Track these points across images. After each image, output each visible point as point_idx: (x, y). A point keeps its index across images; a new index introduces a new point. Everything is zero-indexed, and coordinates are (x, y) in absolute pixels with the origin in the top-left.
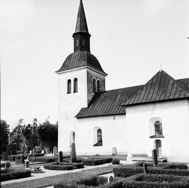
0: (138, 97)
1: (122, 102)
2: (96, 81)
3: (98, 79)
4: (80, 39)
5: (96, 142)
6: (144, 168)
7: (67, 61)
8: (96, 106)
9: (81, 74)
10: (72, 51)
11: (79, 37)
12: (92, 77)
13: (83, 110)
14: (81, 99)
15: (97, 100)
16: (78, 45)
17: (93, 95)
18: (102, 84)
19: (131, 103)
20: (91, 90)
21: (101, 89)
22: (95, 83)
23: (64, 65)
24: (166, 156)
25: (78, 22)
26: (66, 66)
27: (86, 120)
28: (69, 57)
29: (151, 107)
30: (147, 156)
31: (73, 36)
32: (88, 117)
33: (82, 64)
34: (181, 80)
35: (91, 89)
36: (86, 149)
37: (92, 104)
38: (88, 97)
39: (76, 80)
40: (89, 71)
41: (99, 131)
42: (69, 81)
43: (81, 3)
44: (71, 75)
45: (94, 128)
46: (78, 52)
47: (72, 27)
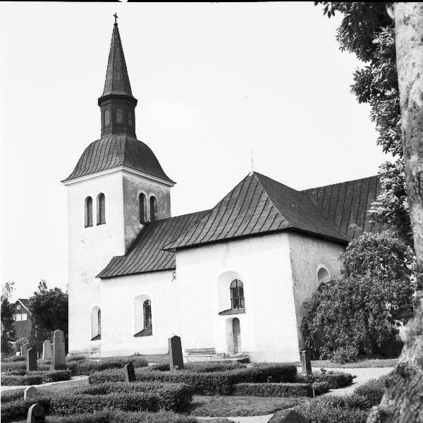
0: (198, 231)
1: (166, 244)
2: (148, 197)
3: (154, 195)
4: (112, 109)
5: (141, 327)
6: (124, 371)
7: (85, 157)
8: (143, 251)
9: (111, 183)
10: (96, 134)
11: (110, 105)
12: (136, 191)
13: (116, 261)
14: (113, 238)
15: (146, 239)
16: (108, 122)
17: (139, 228)
18: (163, 205)
19: (183, 244)
20: (135, 218)
21: (161, 215)
22: (145, 202)
23: (78, 167)
24: (248, 350)
25: (109, 74)
26: (88, 164)
27: (119, 280)
28: (90, 150)
29: (220, 250)
30: (214, 353)
31: (99, 104)
32: (122, 275)
33: (113, 162)
34: (312, 190)
35: (134, 217)
36: (120, 342)
37: (135, 249)
38: (125, 233)
39: (102, 197)
40: (129, 177)
41: (147, 308)
42: (89, 200)
43: (116, 25)
44: (92, 185)
45: (136, 298)
46: (110, 137)
47: (97, 83)
